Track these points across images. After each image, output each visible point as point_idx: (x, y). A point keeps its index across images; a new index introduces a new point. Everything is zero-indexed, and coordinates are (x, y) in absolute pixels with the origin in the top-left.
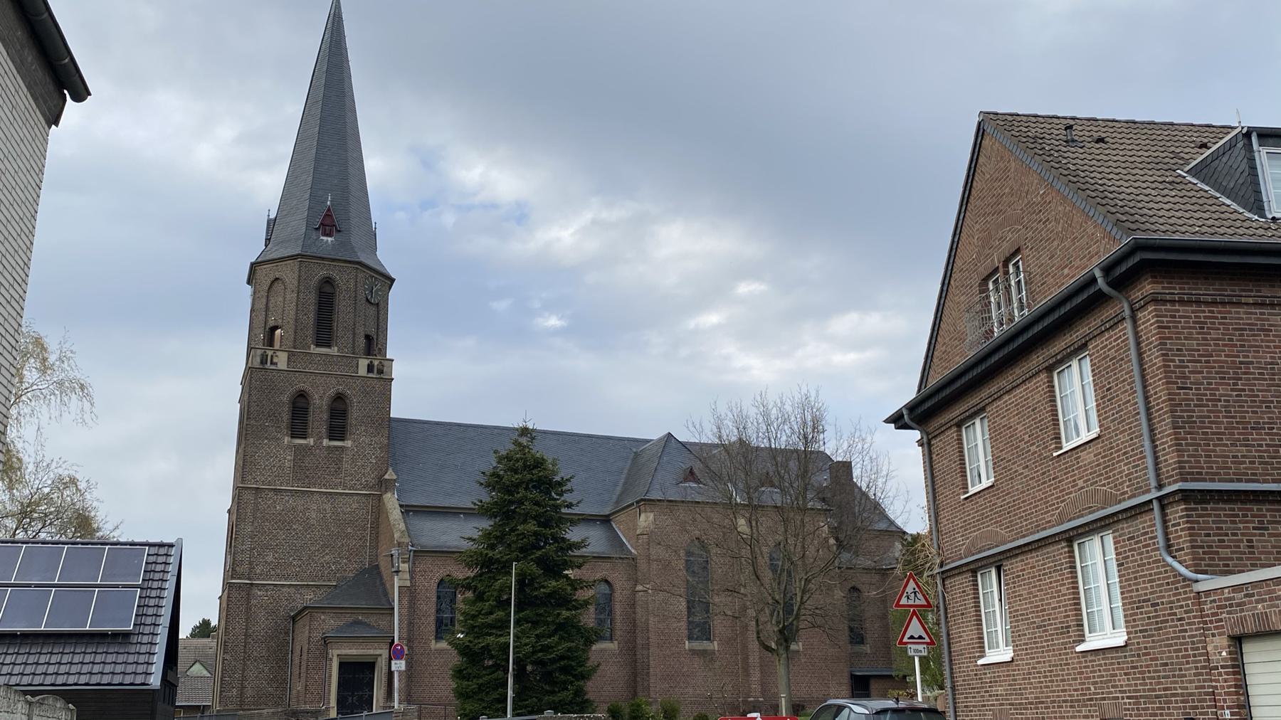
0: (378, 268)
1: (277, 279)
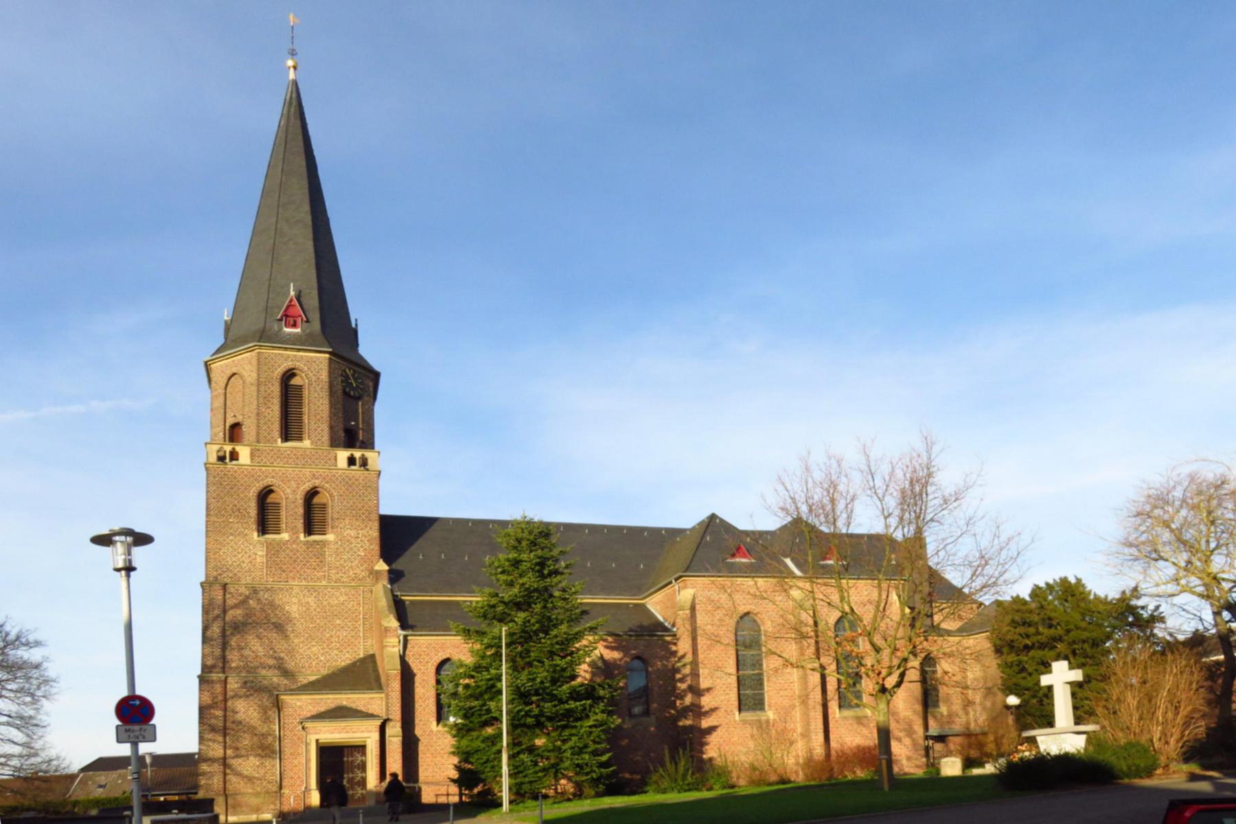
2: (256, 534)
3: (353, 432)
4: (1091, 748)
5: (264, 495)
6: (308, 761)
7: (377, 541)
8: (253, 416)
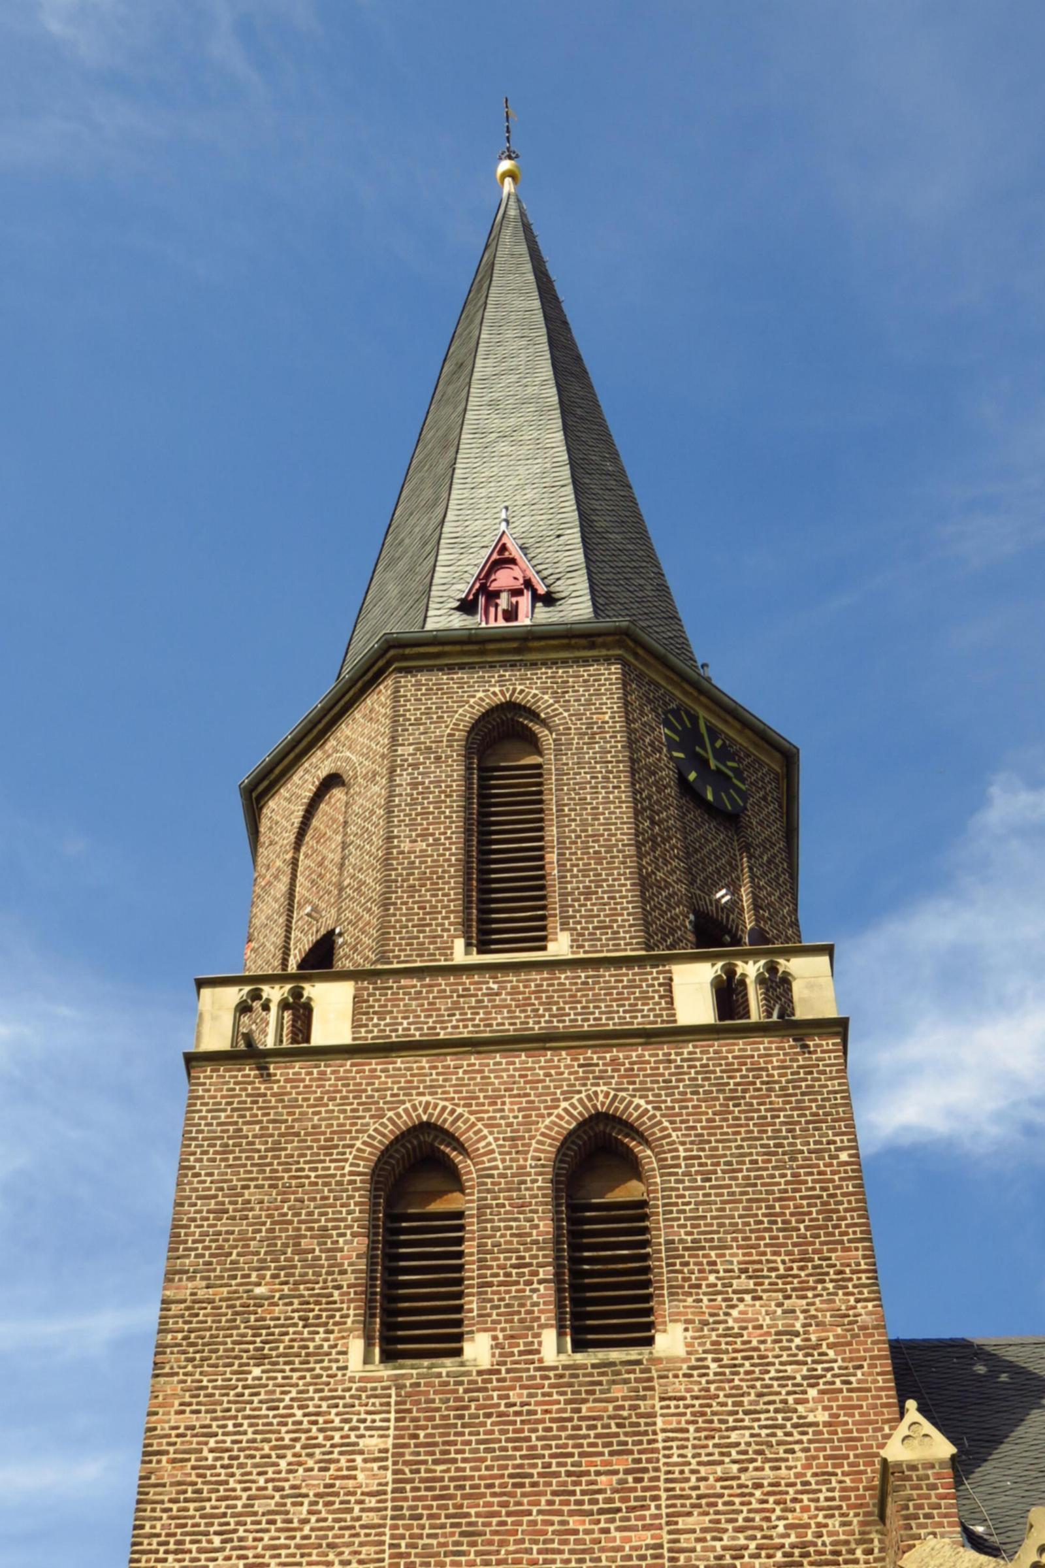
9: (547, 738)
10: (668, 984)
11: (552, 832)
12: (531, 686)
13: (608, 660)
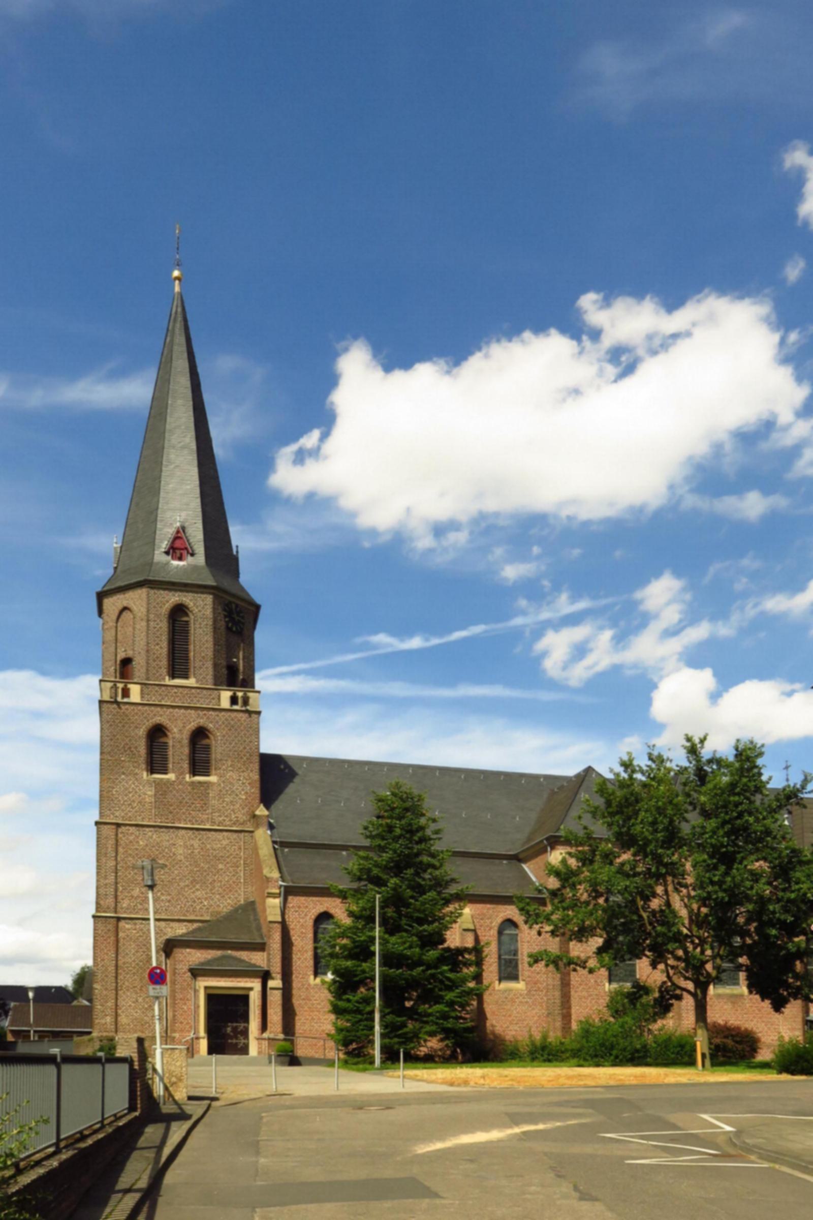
0: (240, 593)
1: (125, 609)
2: (145, 774)
3: (236, 675)
4: (767, 291)
5: (157, 733)
6: (197, 1007)
7: (258, 785)
8: (143, 653)
9: (190, 614)
10: (219, 696)
11: (191, 647)
12: (187, 599)
13: (210, 593)
